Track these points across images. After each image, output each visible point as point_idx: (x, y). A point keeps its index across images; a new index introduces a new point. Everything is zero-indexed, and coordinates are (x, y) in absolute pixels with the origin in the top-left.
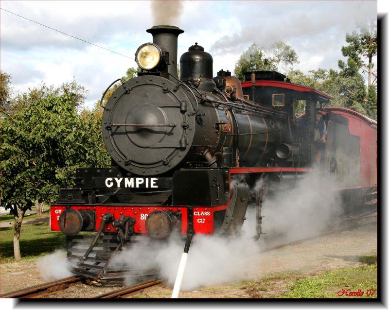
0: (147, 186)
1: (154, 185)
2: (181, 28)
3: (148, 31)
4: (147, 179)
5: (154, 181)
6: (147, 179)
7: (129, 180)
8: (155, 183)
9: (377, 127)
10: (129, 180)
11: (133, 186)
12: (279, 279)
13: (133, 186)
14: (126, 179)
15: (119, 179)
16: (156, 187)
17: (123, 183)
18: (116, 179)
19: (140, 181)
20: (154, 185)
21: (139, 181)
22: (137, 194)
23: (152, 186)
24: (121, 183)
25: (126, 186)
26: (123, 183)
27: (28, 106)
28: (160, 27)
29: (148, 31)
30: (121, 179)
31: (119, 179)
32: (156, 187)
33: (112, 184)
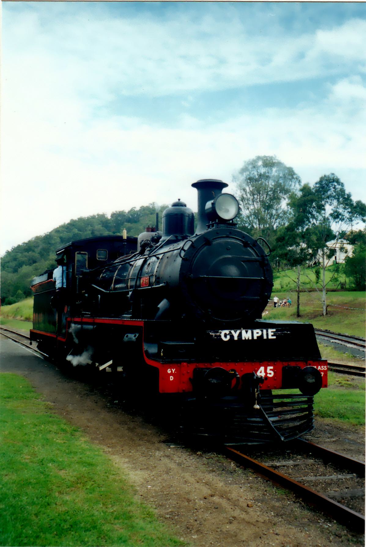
0: (265, 337)
1: (272, 336)
2: (224, 181)
3: (194, 185)
4: (265, 331)
5: (272, 332)
6: (265, 331)
7: (247, 332)
8: (273, 334)
9: (316, 332)
10: (247, 332)
11: (250, 338)
12: (343, 416)
13: (250, 338)
14: (244, 332)
15: (235, 332)
16: (275, 337)
17: (240, 335)
18: (233, 332)
19: (258, 333)
20: (272, 336)
21: (257, 333)
22: (316, 321)
23: (270, 337)
24: (238, 336)
25: (243, 338)
26: (240, 335)
27: (190, 487)
28: (200, 196)
29: (194, 185)
30: (238, 332)
31: (235, 332)
32: (275, 337)
33: (228, 337)
